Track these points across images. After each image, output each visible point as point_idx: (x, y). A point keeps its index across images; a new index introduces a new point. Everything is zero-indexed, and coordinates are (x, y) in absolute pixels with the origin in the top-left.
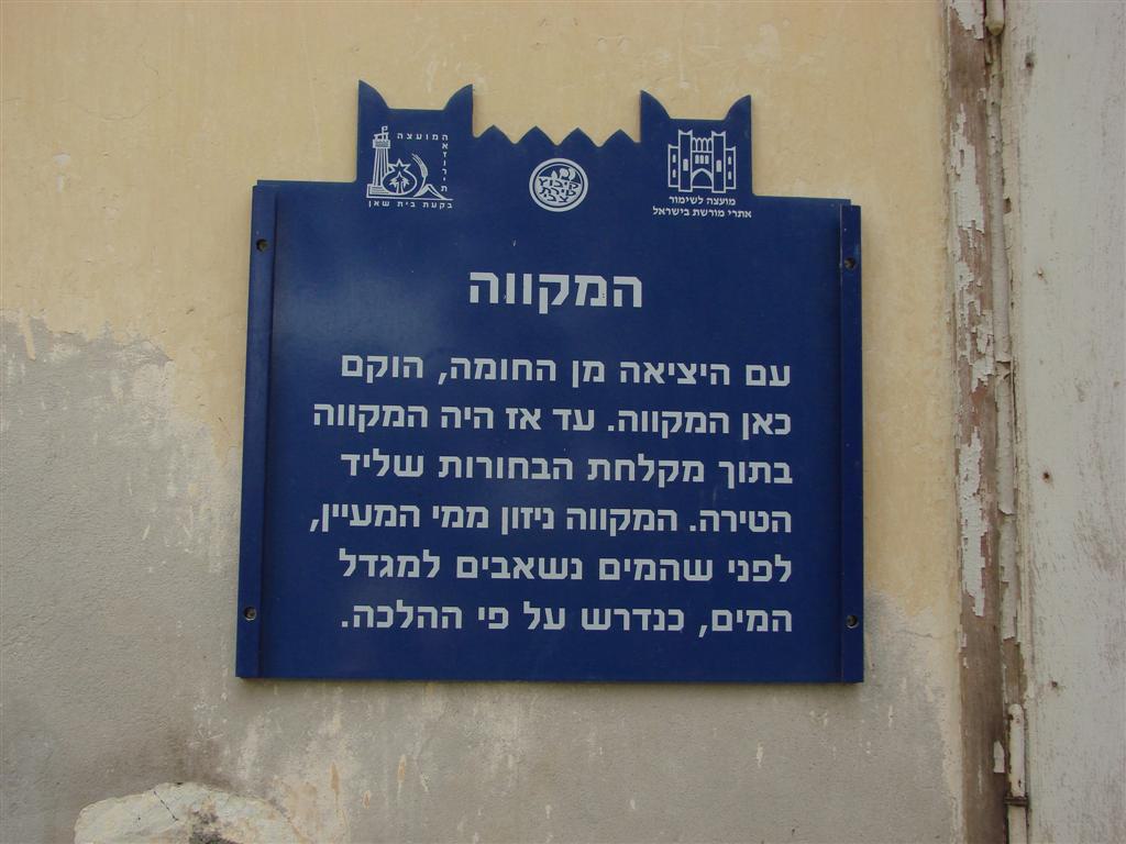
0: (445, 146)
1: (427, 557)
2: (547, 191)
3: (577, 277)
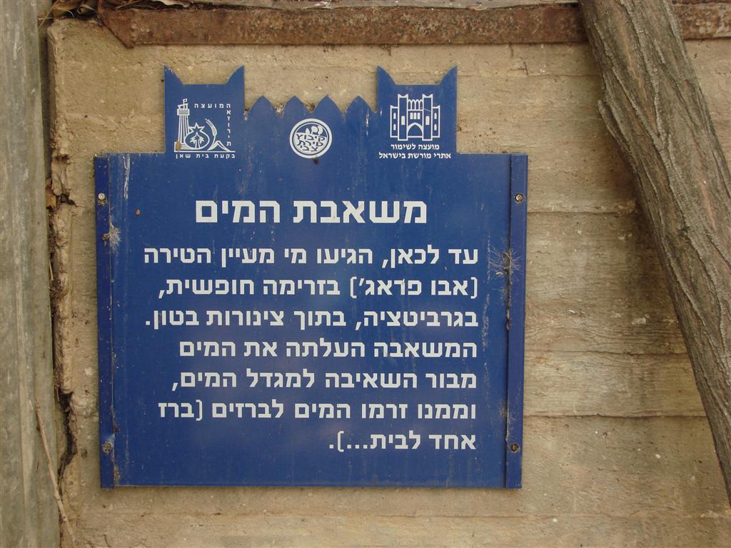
0: (229, 112)
1: (306, 374)
2: (302, 144)
3: (233, 202)
